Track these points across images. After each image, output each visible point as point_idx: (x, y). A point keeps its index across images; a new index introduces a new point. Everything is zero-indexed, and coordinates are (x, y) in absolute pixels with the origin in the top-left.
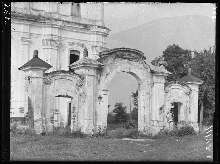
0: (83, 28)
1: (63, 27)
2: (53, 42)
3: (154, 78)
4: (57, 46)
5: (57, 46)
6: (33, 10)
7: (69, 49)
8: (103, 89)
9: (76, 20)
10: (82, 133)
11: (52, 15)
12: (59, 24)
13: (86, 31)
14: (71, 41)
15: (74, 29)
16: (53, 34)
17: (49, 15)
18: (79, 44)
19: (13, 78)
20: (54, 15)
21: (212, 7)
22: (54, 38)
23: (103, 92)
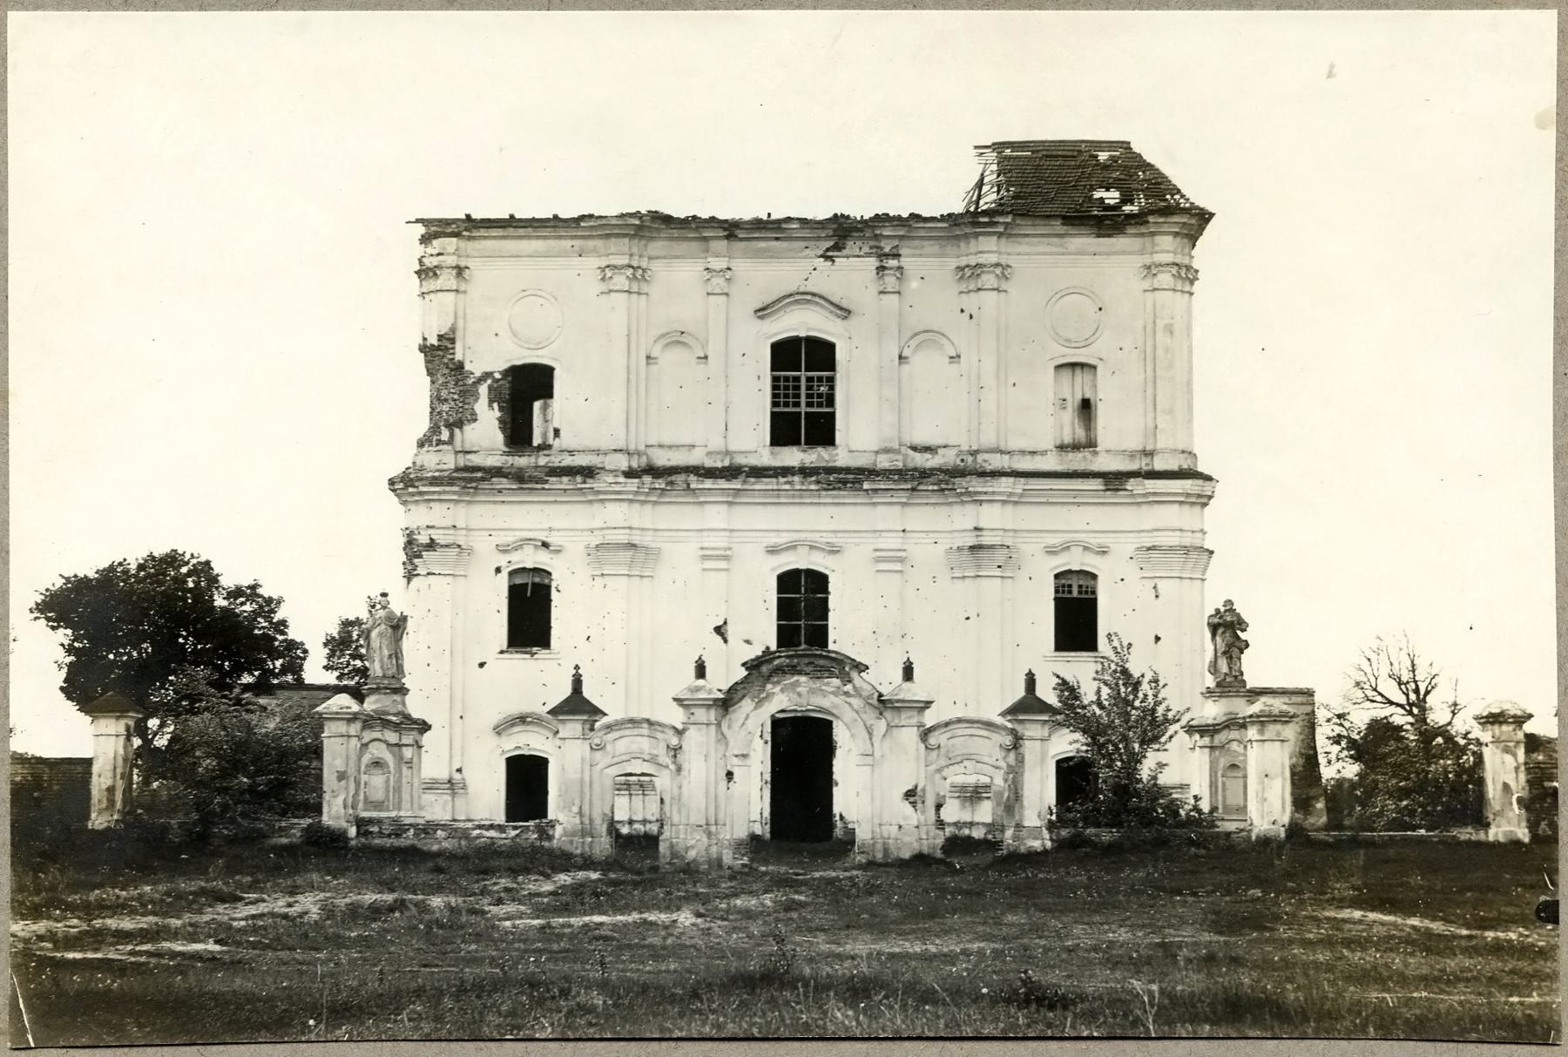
0: (1103, 488)
1: (1021, 495)
2: (983, 554)
3: (888, 714)
4: (999, 567)
5: (999, 567)
6: (914, 448)
7: (1052, 570)
8: (736, 752)
9: (1076, 461)
10: (1136, 769)
11: (980, 457)
12: (1002, 490)
13: (1110, 497)
14: (1056, 540)
15: (1087, 497)
16: (981, 525)
17: (970, 459)
18: (1086, 548)
19: (3, 785)
20: (986, 456)
21: (1547, 19)
22: (987, 539)
23: (735, 761)
